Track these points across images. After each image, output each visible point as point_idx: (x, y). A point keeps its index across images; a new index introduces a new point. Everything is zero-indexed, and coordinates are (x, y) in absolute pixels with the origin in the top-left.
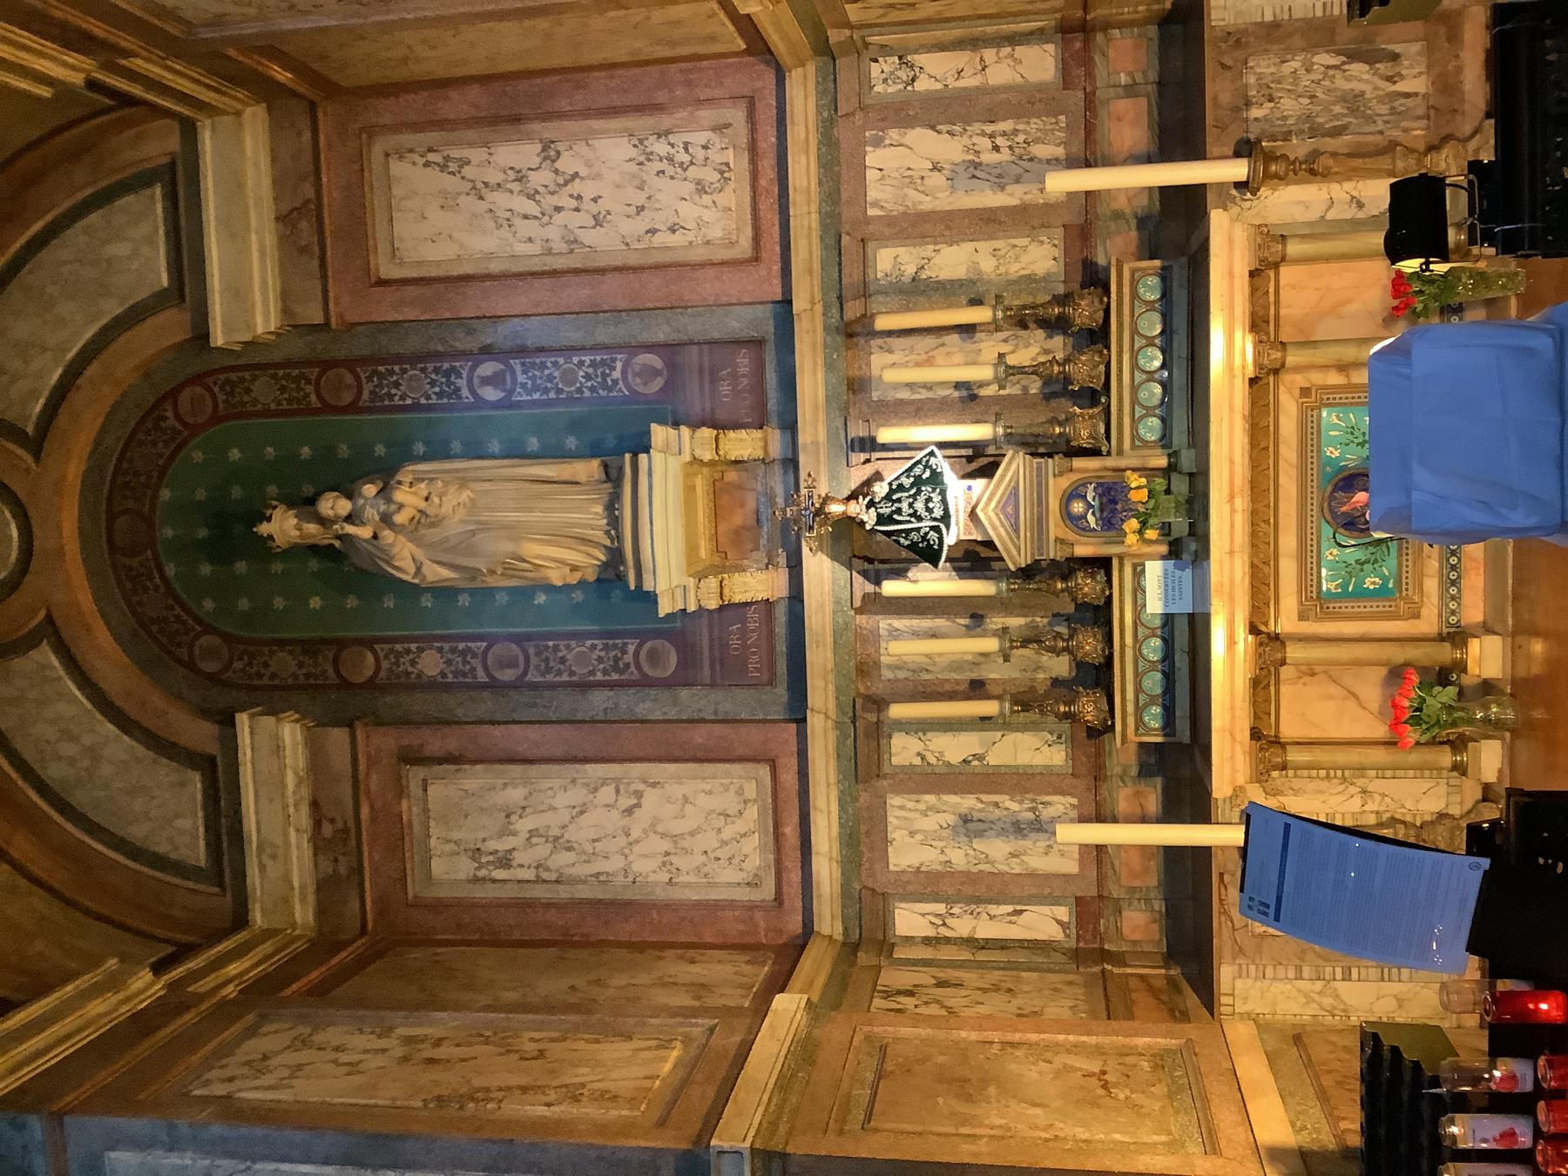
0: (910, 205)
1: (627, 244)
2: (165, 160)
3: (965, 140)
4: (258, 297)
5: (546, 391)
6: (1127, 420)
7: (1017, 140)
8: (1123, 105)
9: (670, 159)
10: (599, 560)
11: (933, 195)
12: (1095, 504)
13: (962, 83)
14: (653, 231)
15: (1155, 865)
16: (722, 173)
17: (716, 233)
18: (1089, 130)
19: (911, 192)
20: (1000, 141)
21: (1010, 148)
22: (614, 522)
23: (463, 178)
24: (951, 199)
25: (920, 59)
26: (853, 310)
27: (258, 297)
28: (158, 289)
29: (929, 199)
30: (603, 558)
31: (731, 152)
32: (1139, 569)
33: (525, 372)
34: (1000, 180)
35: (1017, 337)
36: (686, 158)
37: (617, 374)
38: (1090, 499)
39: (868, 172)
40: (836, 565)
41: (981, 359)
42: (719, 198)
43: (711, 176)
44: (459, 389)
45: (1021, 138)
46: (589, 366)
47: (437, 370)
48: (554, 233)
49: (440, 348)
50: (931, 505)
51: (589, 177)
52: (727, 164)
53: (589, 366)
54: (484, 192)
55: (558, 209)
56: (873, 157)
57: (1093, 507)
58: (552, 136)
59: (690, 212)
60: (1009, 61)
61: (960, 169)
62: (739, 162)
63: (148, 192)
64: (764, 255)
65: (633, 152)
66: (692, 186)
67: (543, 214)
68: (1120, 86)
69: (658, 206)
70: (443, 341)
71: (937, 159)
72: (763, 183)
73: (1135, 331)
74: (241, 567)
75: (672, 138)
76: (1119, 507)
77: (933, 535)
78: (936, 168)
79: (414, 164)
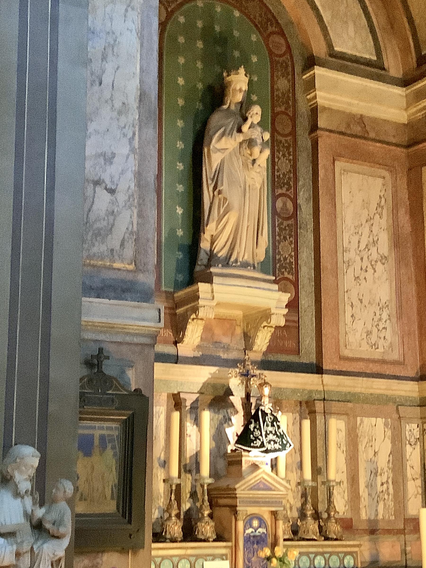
0: (361, 439)
1: (347, 292)
2: (386, 66)
3: (386, 469)
4: (332, 96)
5: (279, 235)
6: (189, 552)
7: (386, 495)
8: (398, 549)
9: (380, 320)
10: (218, 252)
11: (364, 451)
12: (257, 533)
13: (408, 467)
14: (352, 306)
15: (420, 565)
16: (375, 344)
17: (351, 338)
18: (389, 532)
19: (366, 440)
20: (385, 486)
21: (382, 491)
22: (245, 265)
23: (375, 214)
24: (363, 460)
25: (418, 447)
26: (319, 406)
27: (332, 96)
28: (334, 45)
29: (363, 449)
30: (219, 255)
31: (382, 350)
32: (224, 557)
33: (288, 225)
34: (370, 486)
35: (298, 492)
36: (381, 328)
37: (286, 275)
38: (260, 530)
39: (374, 419)
40: (201, 385)
41: (289, 472)
42: (364, 343)
43: (374, 339)
44: (281, 188)
45: (386, 497)
46: (290, 261)
47: (289, 178)
48: (351, 255)
49: (300, 183)
50: (272, 443)
51: (374, 278)
52: (378, 348)
53: (290, 261)
54: (370, 223)
55: (362, 259)
56: (380, 421)
57: (255, 531)
58: (390, 260)
59: (359, 326)
60: (416, 492)
61: (375, 466)
62: (377, 355)
63: (374, 53)
64: (342, 362)
65: (383, 301)
66: (369, 329)
67: (360, 251)
68: (405, 546)
69: (362, 310)
70: (304, 185)
71: (379, 454)
72: (371, 365)
73: (316, 554)
74: (200, 44)
75: (388, 321)
76: (255, 546)
77: (259, 443)
78: (375, 453)
79: (381, 191)
